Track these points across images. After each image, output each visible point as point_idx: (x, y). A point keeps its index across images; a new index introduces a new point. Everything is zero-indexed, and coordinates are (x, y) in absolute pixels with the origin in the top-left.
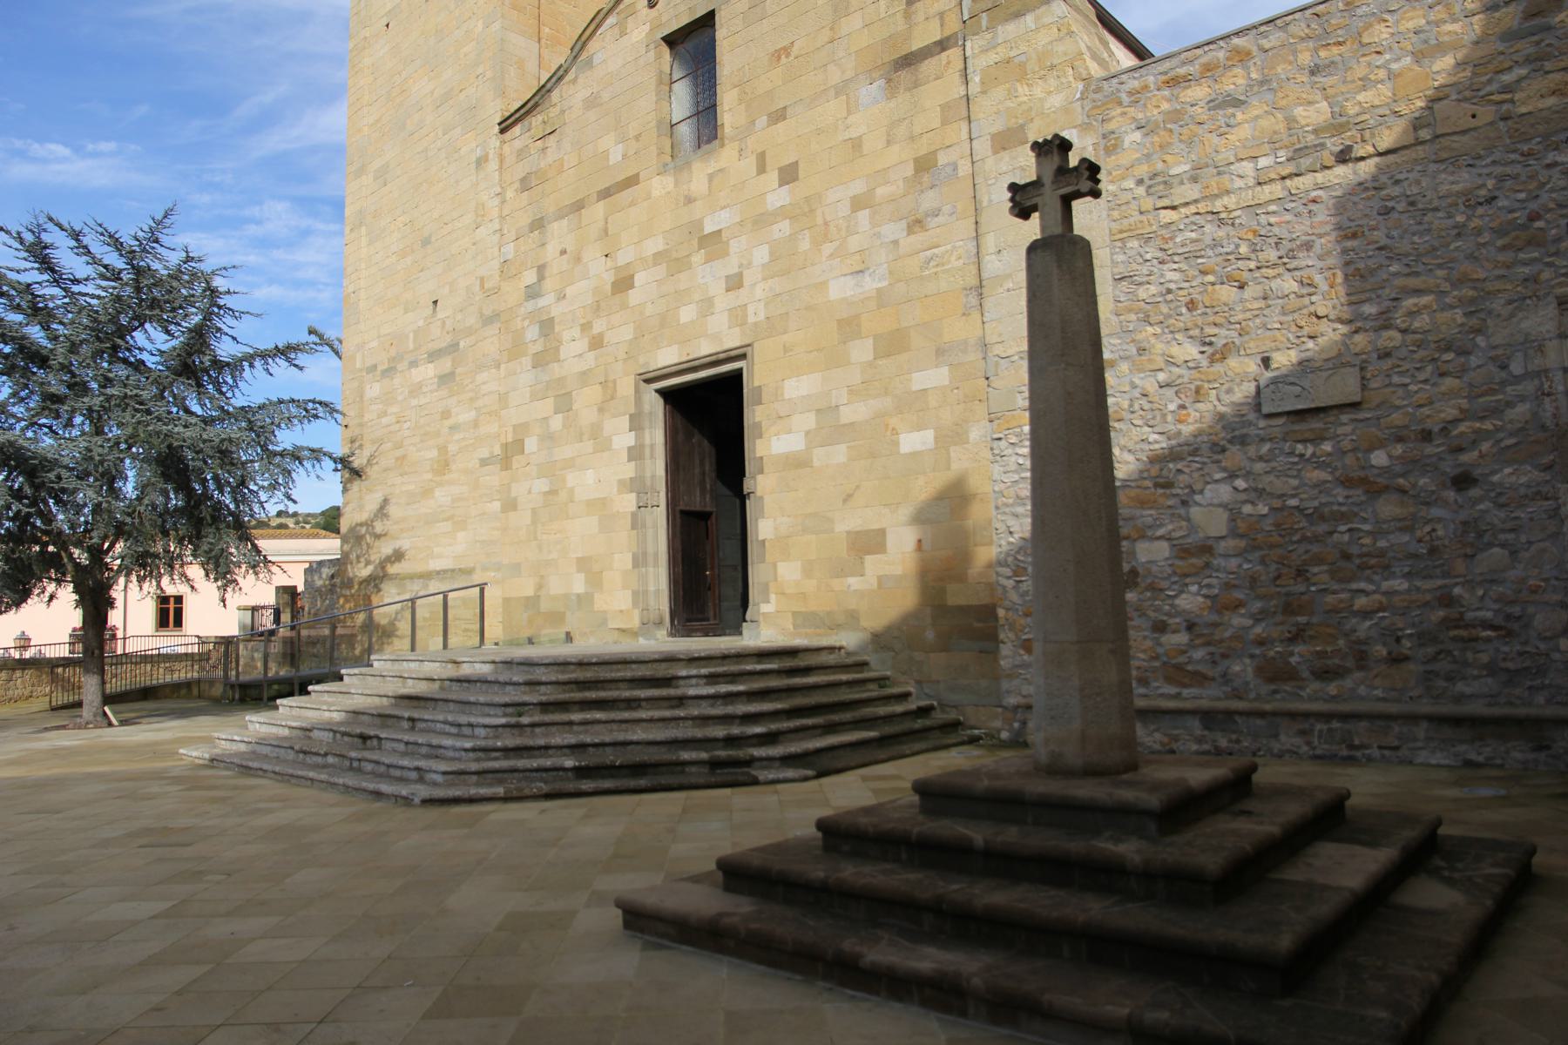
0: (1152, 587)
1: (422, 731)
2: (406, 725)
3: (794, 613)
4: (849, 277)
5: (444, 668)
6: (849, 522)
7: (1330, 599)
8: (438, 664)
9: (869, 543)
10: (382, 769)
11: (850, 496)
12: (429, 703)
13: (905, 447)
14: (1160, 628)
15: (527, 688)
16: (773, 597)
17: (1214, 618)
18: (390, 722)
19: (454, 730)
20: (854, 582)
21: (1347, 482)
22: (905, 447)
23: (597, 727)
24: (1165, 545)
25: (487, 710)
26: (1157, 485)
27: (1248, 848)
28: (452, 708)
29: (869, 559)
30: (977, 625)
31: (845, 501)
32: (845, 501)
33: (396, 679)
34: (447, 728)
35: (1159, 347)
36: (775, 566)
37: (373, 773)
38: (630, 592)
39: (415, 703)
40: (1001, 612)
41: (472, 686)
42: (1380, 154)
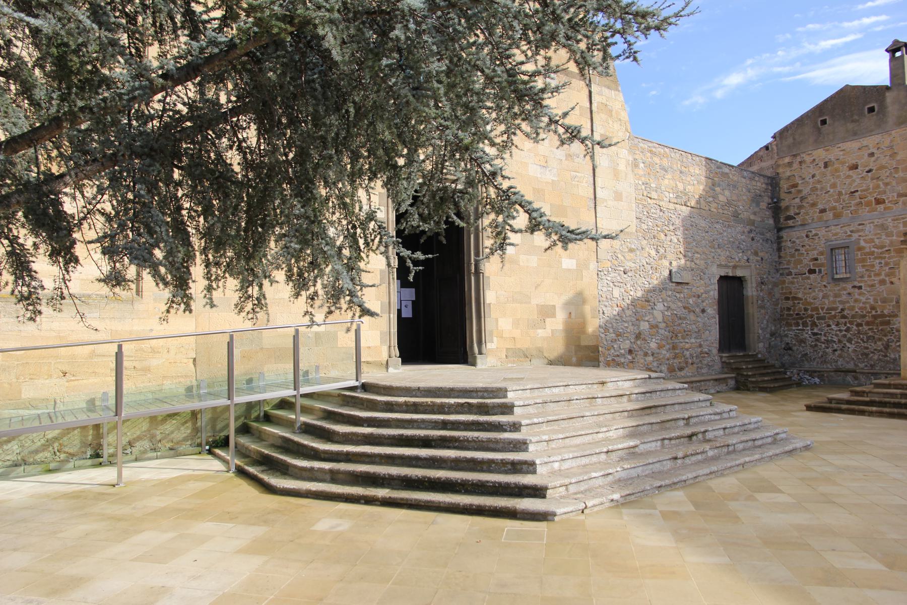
0: (644, 339)
1: (696, 424)
2: (682, 423)
3: (507, 349)
4: (538, 167)
5: (589, 388)
6: (537, 300)
7: (681, 344)
8: (584, 386)
9: (547, 312)
10: (750, 444)
11: (539, 285)
12: (659, 408)
13: (564, 266)
14: (646, 354)
15: (716, 383)
16: (495, 339)
17: (658, 351)
18: (668, 425)
19: (717, 417)
20: (541, 333)
21: (685, 308)
22: (564, 266)
23: (692, 406)
24: (647, 323)
25: (700, 404)
26: (646, 301)
27: (419, 476)
28: (677, 409)
29: (548, 320)
30: (592, 354)
31: (536, 288)
32: (536, 288)
33: (582, 401)
34: (713, 417)
35: (647, 249)
36: (497, 320)
37: (744, 450)
38: (379, 333)
39: (648, 411)
40: (600, 349)
41: (653, 395)
42: (692, 207)
